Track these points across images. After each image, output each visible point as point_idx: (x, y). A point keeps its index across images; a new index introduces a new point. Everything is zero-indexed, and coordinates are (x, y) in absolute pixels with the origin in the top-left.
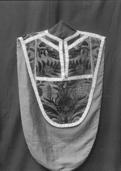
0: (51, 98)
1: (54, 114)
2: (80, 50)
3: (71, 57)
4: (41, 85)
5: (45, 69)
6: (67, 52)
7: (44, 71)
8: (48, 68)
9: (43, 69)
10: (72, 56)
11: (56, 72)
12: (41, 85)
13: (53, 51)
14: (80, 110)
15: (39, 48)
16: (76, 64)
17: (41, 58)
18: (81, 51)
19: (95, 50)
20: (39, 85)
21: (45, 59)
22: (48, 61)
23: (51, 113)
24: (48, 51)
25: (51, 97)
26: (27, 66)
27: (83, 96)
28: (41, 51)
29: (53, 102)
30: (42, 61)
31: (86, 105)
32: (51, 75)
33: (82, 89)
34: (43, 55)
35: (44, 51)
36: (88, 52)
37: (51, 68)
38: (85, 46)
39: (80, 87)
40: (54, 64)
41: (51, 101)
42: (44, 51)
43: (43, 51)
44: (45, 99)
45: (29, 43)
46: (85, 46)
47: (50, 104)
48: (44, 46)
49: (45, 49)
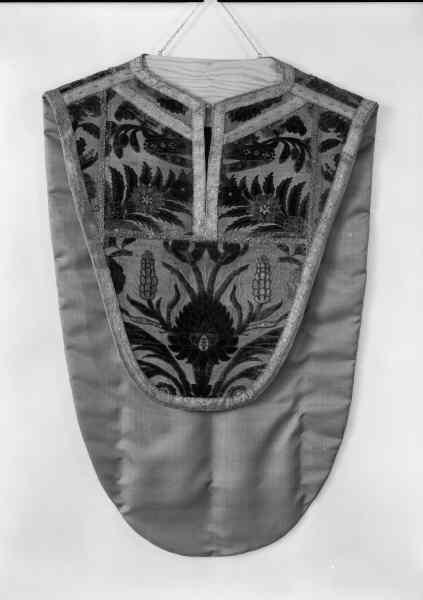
0: (154, 302)
1: (160, 357)
2: (275, 144)
4: (120, 253)
5: (135, 197)
6: (217, 148)
7: (131, 202)
8: (144, 192)
9: (129, 196)
10: (241, 163)
11: (173, 210)
12: (120, 253)
13: (164, 135)
14: (255, 356)
15: (114, 125)
18: (276, 150)
19: (331, 152)
20: (114, 254)
21: (138, 158)
23: (149, 356)
24: (145, 134)
25: (154, 297)
26: (203, 150)
27: (268, 306)
29: (159, 316)
31: (277, 341)
32: (157, 218)
33: (268, 283)
34: (128, 150)
35: (134, 134)
36: (303, 155)
37: (157, 194)
38: (291, 135)
39: (263, 275)
41: (151, 311)
42: (134, 134)
44: (133, 303)
45: (79, 107)
46: (291, 135)
47: (141, 323)
48: (133, 118)
49: (137, 128)
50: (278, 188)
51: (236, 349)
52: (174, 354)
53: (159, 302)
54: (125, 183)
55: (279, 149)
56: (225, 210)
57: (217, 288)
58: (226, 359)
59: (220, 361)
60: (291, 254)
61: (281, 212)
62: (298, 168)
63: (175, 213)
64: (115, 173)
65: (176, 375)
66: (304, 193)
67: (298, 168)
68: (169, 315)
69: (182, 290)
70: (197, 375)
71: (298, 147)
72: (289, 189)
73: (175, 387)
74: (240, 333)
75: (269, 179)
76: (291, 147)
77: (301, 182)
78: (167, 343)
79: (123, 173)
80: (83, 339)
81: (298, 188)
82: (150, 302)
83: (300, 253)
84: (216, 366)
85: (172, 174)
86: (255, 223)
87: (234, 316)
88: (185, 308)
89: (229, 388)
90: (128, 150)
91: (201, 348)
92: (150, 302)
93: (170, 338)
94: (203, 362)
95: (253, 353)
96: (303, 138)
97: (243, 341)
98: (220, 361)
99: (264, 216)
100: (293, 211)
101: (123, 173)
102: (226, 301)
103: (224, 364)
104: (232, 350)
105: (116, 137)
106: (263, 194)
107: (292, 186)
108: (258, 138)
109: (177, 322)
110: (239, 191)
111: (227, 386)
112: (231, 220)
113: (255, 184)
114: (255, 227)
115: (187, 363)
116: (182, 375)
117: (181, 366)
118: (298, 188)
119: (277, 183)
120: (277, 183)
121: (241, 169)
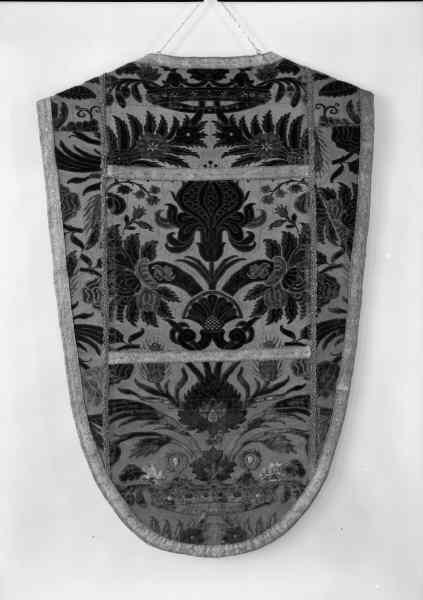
0: (162, 384)
2: (270, 86)
17: (127, 108)
23: (160, 428)
24: (146, 86)
28: (123, 85)
29: (167, 395)
30: (131, 117)
34: (130, 100)
38: (286, 75)
40: (170, 125)
44: (141, 386)
46: (286, 75)
50: (277, 124)
51: (245, 420)
53: (166, 386)
54: (131, 133)
56: (226, 149)
62: (294, 104)
63: (181, 157)
64: (120, 123)
66: (304, 126)
67: (294, 104)
68: (177, 391)
71: (292, 84)
75: (268, 117)
76: (286, 85)
79: (127, 121)
80: (73, 196)
81: (298, 122)
85: (176, 121)
87: (241, 390)
90: (130, 100)
92: (158, 385)
96: (296, 77)
99: (267, 154)
100: (294, 143)
101: (127, 121)
105: (117, 89)
107: (291, 120)
108: (252, 82)
109: (186, 398)
113: (255, 122)
118: (298, 122)
119: (275, 120)
120: (275, 120)
121: (240, 109)
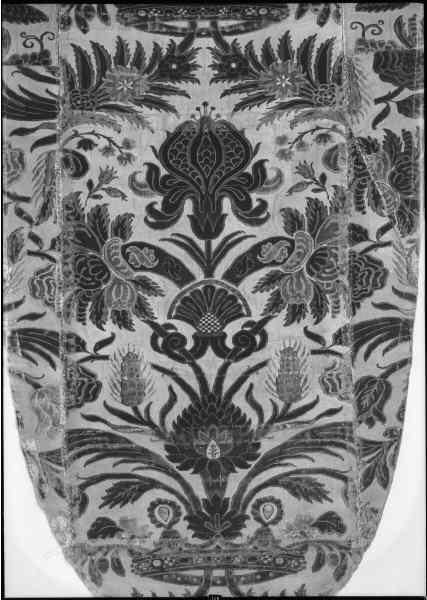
2: (305, 547)
3: (256, 574)
4: (92, 358)
16: (260, 59)
22: (121, 45)
29: (150, 423)
30: (95, 46)
32: (140, 105)
41: (140, 420)
43: (108, 558)
44: (113, 411)
52: (174, 466)
53: (147, 410)
55: (311, 556)
57: (228, 384)
58: (245, 466)
59: (237, 469)
60: (328, 345)
61: (307, 82)
64: (79, 53)
65: (182, 492)
69: (177, 388)
70: (208, 488)
72: (315, 49)
73: (179, 503)
74: (263, 434)
75: (285, 40)
76: (327, 552)
77: (330, 37)
78: (163, 454)
79: (90, 51)
81: (327, 47)
82: (135, 409)
83: (341, 343)
84: (232, 476)
86: (272, 98)
88: (184, 412)
89: (253, 501)
91: (210, 457)
92: (135, 409)
93: (167, 448)
94: (214, 472)
95: (281, 459)
97: (267, 446)
98: (237, 469)
100: (322, 75)
101: (90, 51)
102: (239, 400)
103: (242, 473)
104: (254, 458)
106: (279, 61)
107: (317, 44)
110: (246, 62)
111: (249, 498)
112: (237, 98)
114: (273, 104)
115: (194, 472)
116: (187, 488)
117: (188, 480)
118: (327, 47)
119: (295, 45)
120: (295, 45)
